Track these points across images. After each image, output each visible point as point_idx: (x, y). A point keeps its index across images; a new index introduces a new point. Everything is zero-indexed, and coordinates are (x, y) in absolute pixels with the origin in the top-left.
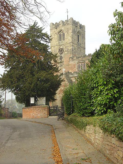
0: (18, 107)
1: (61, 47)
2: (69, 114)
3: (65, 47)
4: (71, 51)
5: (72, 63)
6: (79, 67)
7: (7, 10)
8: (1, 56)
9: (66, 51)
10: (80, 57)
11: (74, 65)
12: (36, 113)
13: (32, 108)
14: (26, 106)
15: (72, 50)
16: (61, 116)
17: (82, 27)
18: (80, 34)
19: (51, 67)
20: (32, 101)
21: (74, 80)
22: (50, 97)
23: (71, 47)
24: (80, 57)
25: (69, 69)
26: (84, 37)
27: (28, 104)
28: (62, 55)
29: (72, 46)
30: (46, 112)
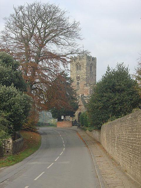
0: (53, 121)
1: (78, 76)
2: (83, 126)
3: (82, 76)
4: (86, 79)
5: (85, 88)
6: (91, 92)
7: (47, 58)
8: (1, 50)
9: (82, 79)
10: (92, 85)
11: (88, 90)
12: (65, 124)
13: (63, 122)
14: (58, 120)
15: (86, 78)
16: (79, 127)
17: (94, 59)
18: (92, 65)
19: (73, 98)
20: (62, 118)
21: (86, 101)
22: (72, 115)
23: (86, 76)
24: (92, 85)
25: (84, 92)
26: (95, 67)
27: (60, 120)
28: (79, 82)
29: (86, 75)
30: (71, 124)
